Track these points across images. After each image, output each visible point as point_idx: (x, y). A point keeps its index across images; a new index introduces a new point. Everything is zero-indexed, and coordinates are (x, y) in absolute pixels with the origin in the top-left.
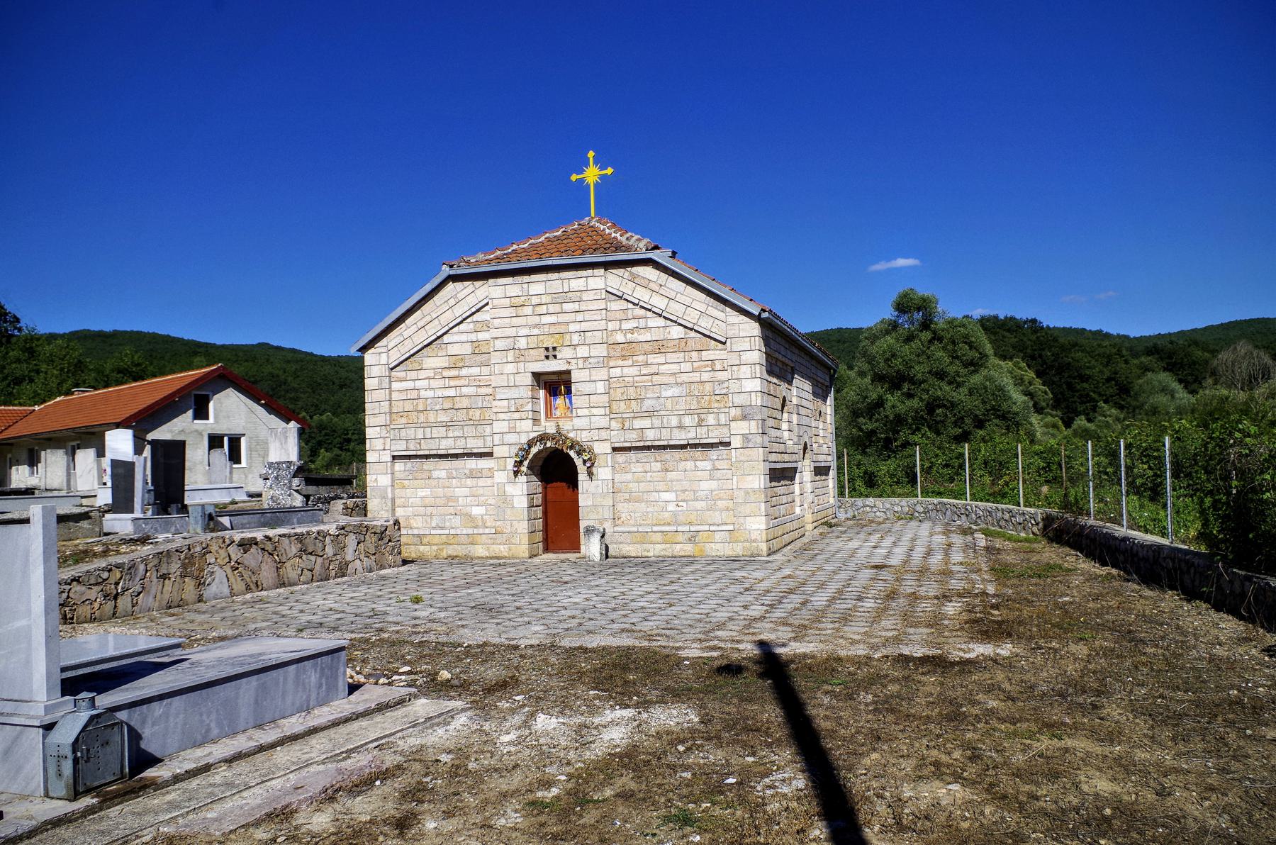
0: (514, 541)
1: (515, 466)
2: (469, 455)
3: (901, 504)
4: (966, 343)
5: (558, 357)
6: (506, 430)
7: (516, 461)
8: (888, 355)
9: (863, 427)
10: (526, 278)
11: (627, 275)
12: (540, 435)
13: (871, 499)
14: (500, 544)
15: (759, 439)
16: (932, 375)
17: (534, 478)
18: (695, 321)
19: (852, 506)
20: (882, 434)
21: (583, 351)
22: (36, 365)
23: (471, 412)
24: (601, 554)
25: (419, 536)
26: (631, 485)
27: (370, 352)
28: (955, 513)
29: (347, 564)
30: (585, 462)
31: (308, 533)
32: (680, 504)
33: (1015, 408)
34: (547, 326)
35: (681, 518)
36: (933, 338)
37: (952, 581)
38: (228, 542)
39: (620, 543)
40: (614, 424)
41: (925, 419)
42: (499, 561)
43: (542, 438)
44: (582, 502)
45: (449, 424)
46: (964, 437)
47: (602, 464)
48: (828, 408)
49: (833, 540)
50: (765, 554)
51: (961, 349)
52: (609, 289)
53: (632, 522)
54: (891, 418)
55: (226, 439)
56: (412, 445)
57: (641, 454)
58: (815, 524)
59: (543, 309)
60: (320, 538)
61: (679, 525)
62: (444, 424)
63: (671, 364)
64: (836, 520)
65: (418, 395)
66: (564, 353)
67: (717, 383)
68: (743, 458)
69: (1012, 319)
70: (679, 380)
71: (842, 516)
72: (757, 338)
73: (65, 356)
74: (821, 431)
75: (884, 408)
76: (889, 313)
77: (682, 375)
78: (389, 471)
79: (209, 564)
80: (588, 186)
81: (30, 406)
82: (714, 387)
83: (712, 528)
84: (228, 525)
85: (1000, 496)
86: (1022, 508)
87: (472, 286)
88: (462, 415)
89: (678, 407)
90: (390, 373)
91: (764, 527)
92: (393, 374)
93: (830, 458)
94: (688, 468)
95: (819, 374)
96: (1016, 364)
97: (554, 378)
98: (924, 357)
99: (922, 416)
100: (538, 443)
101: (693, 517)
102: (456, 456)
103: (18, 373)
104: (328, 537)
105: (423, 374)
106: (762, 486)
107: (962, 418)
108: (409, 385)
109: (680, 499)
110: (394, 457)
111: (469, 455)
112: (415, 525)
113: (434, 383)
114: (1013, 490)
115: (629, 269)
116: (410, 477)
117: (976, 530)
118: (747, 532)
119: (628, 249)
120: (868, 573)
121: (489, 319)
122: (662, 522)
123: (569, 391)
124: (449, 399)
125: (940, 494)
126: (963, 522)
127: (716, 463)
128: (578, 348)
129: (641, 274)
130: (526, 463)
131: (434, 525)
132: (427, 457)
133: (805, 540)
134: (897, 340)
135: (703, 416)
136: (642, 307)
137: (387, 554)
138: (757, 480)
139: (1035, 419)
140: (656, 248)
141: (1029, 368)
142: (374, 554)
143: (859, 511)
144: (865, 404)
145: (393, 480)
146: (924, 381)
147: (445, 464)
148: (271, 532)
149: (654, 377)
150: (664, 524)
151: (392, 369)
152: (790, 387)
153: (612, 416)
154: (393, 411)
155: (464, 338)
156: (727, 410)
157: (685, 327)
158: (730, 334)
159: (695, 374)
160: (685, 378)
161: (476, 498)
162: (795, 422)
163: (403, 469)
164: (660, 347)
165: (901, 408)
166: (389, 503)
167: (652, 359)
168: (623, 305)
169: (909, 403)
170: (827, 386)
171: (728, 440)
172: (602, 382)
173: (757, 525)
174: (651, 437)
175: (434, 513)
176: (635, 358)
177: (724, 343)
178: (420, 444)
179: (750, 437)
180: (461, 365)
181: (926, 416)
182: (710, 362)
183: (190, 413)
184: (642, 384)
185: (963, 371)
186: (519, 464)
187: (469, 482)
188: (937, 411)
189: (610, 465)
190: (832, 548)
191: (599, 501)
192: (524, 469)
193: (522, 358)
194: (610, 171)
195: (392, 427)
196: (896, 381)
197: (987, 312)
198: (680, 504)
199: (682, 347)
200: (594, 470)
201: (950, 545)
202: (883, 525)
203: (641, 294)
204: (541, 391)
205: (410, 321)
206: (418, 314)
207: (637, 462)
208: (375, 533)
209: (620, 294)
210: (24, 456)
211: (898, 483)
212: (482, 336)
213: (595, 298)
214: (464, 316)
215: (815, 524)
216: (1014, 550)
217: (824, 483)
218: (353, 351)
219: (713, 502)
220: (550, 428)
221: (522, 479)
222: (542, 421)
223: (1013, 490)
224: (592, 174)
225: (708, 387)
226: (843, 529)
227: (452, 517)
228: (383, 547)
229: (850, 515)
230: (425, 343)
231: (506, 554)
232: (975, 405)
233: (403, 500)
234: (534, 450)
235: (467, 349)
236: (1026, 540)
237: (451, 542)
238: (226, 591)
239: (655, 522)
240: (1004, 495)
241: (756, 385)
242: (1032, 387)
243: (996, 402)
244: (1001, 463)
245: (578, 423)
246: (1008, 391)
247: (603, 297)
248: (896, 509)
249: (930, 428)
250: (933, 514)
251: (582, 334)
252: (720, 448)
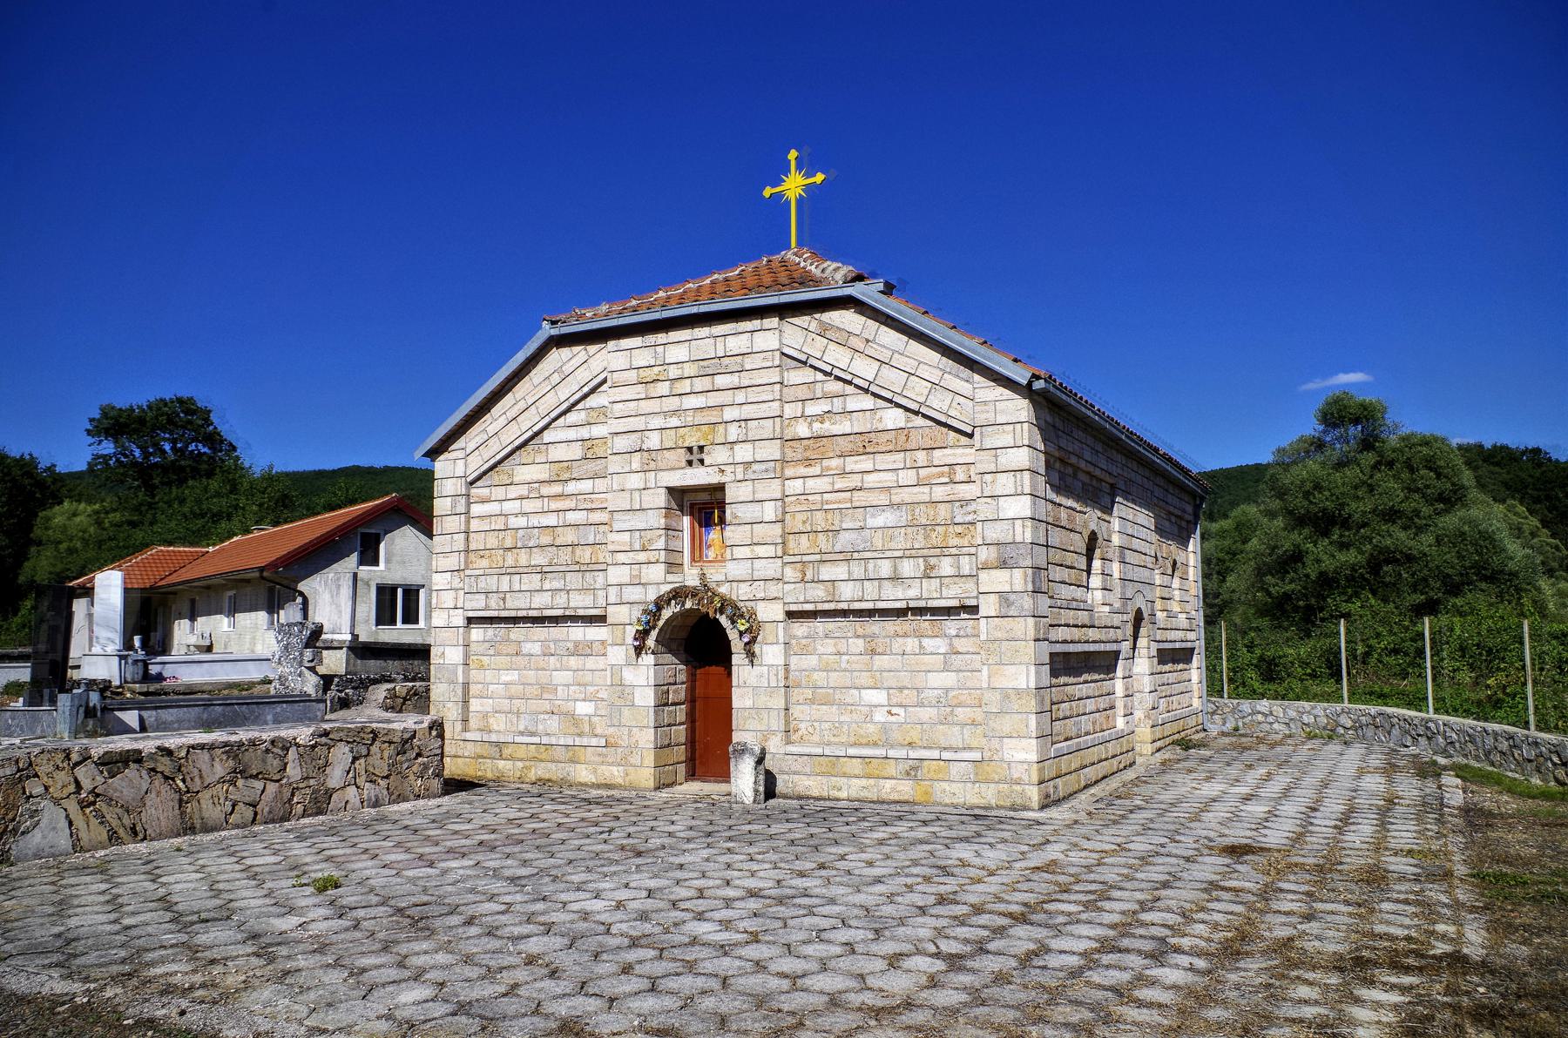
0: (632, 761)
1: (636, 639)
2: (575, 619)
3: (1316, 712)
4: (1431, 469)
5: (706, 463)
6: (626, 580)
7: (637, 631)
8: (1308, 486)
9: (1271, 589)
10: (661, 338)
11: (813, 326)
12: (674, 590)
13: (1265, 702)
14: (612, 764)
15: (1027, 602)
16: (1377, 516)
17: (669, 658)
18: (921, 400)
19: (1233, 711)
20: (1299, 600)
21: (743, 453)
22: (236, 499)
23: (578, 551)
24: (756, 791)
25: (497, 744)
26: (816, 676)
27: (442, 457)
28: (1408, 732)
29: (329, 794)
30: (741, 634)
31: (253, 743)
32: (894, 710)
33: (1511, 566)
34: (691, 413)
35: (896, 736)
36: (1379, 463)
37: (1386, 906)
38: (75, 757)
39: (795, 773)
40: (790, 573)
41: (1366, 580)
42: (610, 793)
43: (678, 594)
44: (736, 703)
45: (545, 569)
46: (1431, 608)
47: (771, 639)
48: (1192, 555)
49: (1179, 778)
50: (1035, 805)
51: (1422, 478)
52: (787, 351)
53: (816, 738)
54: (1313, 576)
55: (400, 591)
56: (494, 601)
57: (831, 625)
58: (1159, 744)
59: (685, 386)
60: (275, 750)
61: (892, 747)
62: (539, 569)
63: (882, 471)
64: (1202, 735)
65: (506, 524)
66: (717, 455)
67: (958, 504)
68: (999, 635)
69: (1504, 448)
70: (896, 499)
71: (1214, 730)
72: (1026, 426)
73: (266, 488)
74: (1177, 593)
75: (1304, 563)
76: (1311, 427)
77: (899, 490)
78: (461, 642)
79: (31, 796)
80: (788, 203)
81: (203, 547)
82: (953, 512)
83: (946, 755)
84: (135, 725)
85: (1487, 707)
86: (1533, 732)
87: (584, 352)
88: (565, 556)
89: (893, 545)
90: (468, 490)
91: (1034, 757)
92: (474, 491)
93: (1192, 636)
94: (908, 650)
95: (1170, 501)
96: (1510, 509)
97: (704, 497)
98: (1365, 489)
99: (1362, 575)
100: (673, 602)
101: (914, 735)
102: (556, 620)
103: (215, 509)
104: (293, 751)
105: (513, 492)
106: (1032, 685)
107: (1425, 580)
108: (493, 508)
109: (894, 701)
110: (470, 620)
111: (575, 619)
112: (495, 727)
113: (529, 506)
114: (1514, 696)
115: (817, 316)
116: (491, 652)
117: (1445, 768)
118: (1005, 766)
119: (816, 282)
120: (1210, 867)
121: (607, 404)
122: (864, 741)
123: (722, 521)
124: (548, 530)
125: (1382, 698)
126: (1422, 749)
127: (956, 642)
128: (737, 447)
129: (837, 323)
130: (654, 634)
131: (521, 728)
132: (514, 620)
133: (1130, 775)
134: (1323, 464)
135: (933, 561)
136: (838, 378)
137: (412, 777)
138: (1024, 675)
139: (1544, 584)
140: (859, 278)
141: (1531, 514)
142: (387, 777)
143: (1245, 720)
144: (1274, 557)
145: (467, 656)
146: (1364, 525)
147: (540, 632)
148: (172, 742)
149: (856, 494)
150: (867, 744)
151: (472, 483)
152: (1107, 518)
153: (787, 559)
154: (471, 548)
155: (572, 434)
156: (973, 550)
157: (907, 409)
158: (981, 419)
159: (922, 489)
160: (905, 495)
161: (582, 689)
162: (1116, 575)
163: (481, 639)
164: (865, 444)
165: (1328, 564)
166: (460, 692)
167: (853, 464)
168: (807, 375)
169: (1342, 557)
170: (1188, 522)
171: (973, 602)
172: (773, 503)
173: (1023, 753)
174: (848, 594)
175: (523, 709)
176: (826, 463)
177: (971, 436)
178: (504, 599)
179: (1012, 597)
180: (566, 476)
181: (1367, 576)
182: (946, 469)
183: (354, 557)
184: (835, 506)
185: (1426, 510)
186: (642, 635)
187: (573, 662)
188: (1385, 568)
189: (781, 640)
190: (1167, 796)
191: (763, 701)
192: (651, 642)
193: (653, 465)
194: (819, 178)
195: (468, 572)
196: (1323, 523)
197: (1470, 440)
198: (894, 710)
199: (901, 442)
200: (757, 648)
201: (1391, 802)
202: (1278, 749)
203: (837, 357)
204: (685, 518)
205: (497, 410)
206: (508, 400)
207: (826, 636)
208: (390, 743)
209: (803, 358)
210: (186, 607)
211: (1313, 676)
212: (597, 431)
213: (764, 365)
214: (572, 400)
215: (1159, 744)
216: (1519, 815)
217: (1185, 675)
218: (416, 459)
219: (949, 709)
220: (691, 578)
221: (648, 659)
222: (686, 566)
223: (1514, 696)
224: (794, 185)
225: (943, 512)
226: (1208, 753)
227: (546, 717)
228: (405, 766)
229: (1229, 726)
230: (517, 443)
231: (620, 781)
232: (1447, 559)
233: (480, 686)
234: (667, 614)
235: (576, 451)
236: (1546, 795)
237: (544, 756)
238: (64, 842)
239: (852, 739)
240: (1497, 704)
241: (1021, 507)
242: (1535, 540)
243: (1480, 554)
244: (1490, 651)
245: (735, 570)
246: (1501, 540)
247: (777, 362)
248: (1306, 719)
249: (1374, 593)
250: (1370, 732)
251: (743, 424)
252: (963, 616)
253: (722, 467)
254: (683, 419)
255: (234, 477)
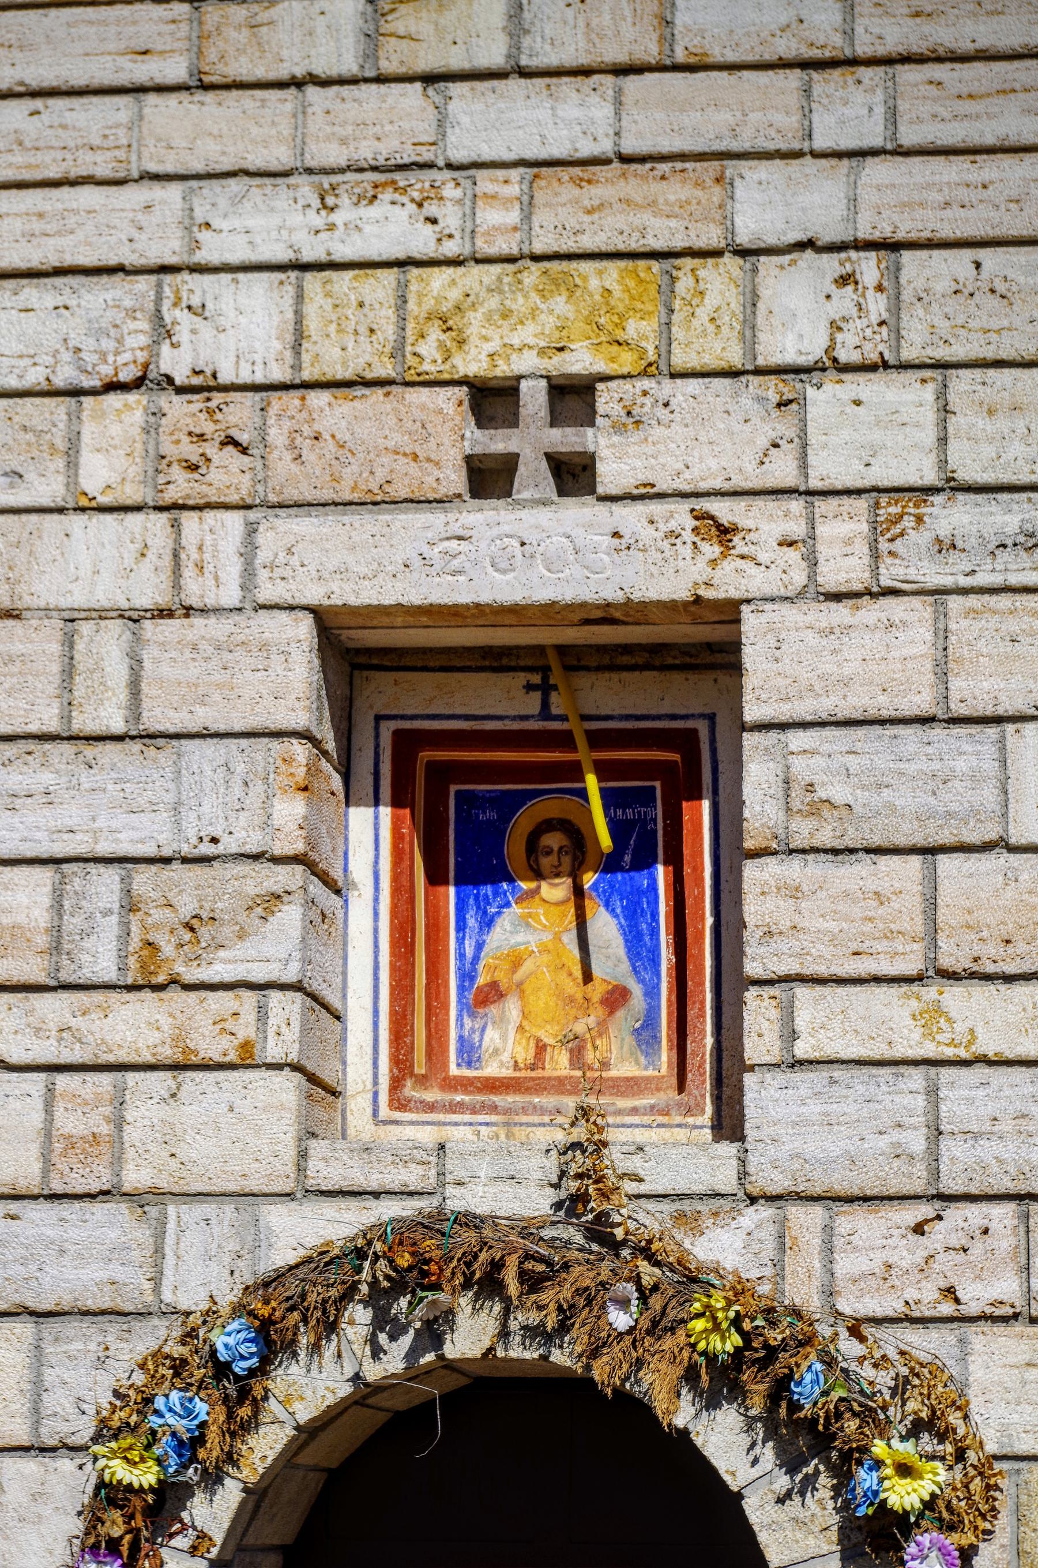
204: (360, 818)
253: (723, 510)
254: (451, 218)
255: (549, 382)
